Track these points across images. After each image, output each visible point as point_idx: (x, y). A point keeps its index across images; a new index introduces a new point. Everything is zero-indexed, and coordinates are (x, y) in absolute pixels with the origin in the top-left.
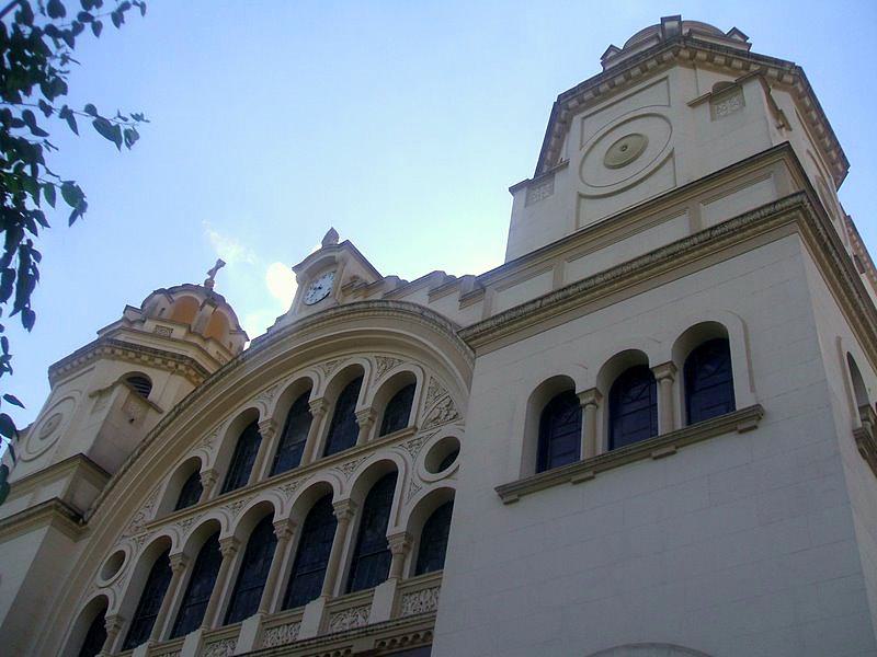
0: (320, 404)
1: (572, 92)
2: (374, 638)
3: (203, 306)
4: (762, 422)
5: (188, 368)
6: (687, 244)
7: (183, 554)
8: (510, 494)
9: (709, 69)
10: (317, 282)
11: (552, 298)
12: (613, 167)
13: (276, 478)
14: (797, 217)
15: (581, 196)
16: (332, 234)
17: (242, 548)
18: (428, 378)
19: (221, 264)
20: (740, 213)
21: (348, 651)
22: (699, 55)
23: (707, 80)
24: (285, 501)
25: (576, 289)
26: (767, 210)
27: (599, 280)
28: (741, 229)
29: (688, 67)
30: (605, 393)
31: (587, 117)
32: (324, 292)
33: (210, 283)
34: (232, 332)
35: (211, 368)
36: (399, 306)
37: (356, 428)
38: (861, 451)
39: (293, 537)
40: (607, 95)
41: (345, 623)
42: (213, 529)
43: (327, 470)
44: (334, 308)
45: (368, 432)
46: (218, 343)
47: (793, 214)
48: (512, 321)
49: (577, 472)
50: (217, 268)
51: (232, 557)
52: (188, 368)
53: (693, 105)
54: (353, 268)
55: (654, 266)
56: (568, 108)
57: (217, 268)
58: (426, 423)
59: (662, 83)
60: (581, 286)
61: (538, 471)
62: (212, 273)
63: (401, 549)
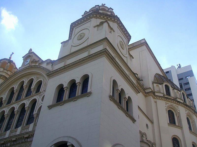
0: (25, 86)
1: (74, 23)
2: (28, 135)
3: (8, 63)
4: (91, 95)
5: (3, 77)
6: (86, 58)
7: (17, 111)
8: (50, 107)
9: (99, 19)
10: (27, 60)
11: (62, 68)
12: (79, 40)
13: (27, 97)
14: (105, 53)
15: (72, 46)
16: (31, 50)
17: (19, 113)
18: (44, 82)
19: (13, 53)
20: (100, 50)
21: (24, 137)
22: (98, 16)
23: (99, 21)
24: (17, 106)
25: (66, 66)
26: (99, 52)
27: (70, 65)
28: (95, 55)
29: (96, 18)
30: (82, 83)
31: (76, 28)
32: (28, 62)
33: (10, 58)
34: (14, 69)
35: (8, 77)
36: (40, 67)
37: (31, 92)
38: (110, 100)
39: (29, 110)
40: (83, 22)
41: (14, 134)
42: (24, 105)
43: (36, 96)
44: (29, 67)
45: (34, 93)
46: (10, 71)
47: (104, 53)
48: (73, 65)
49: (61, 104)
50: (12, 54)
51: (17, 115)
52: (3, 77)
53: (94, 27)
54: (34, 57)
55: (80, 62)
56: (73, 26)
57: (12, 54)
58: (43, 91)
59: (90, 22)
60: (67, 66)
61: (69, 98)
62: (11, 55)
63: (36, 116)
